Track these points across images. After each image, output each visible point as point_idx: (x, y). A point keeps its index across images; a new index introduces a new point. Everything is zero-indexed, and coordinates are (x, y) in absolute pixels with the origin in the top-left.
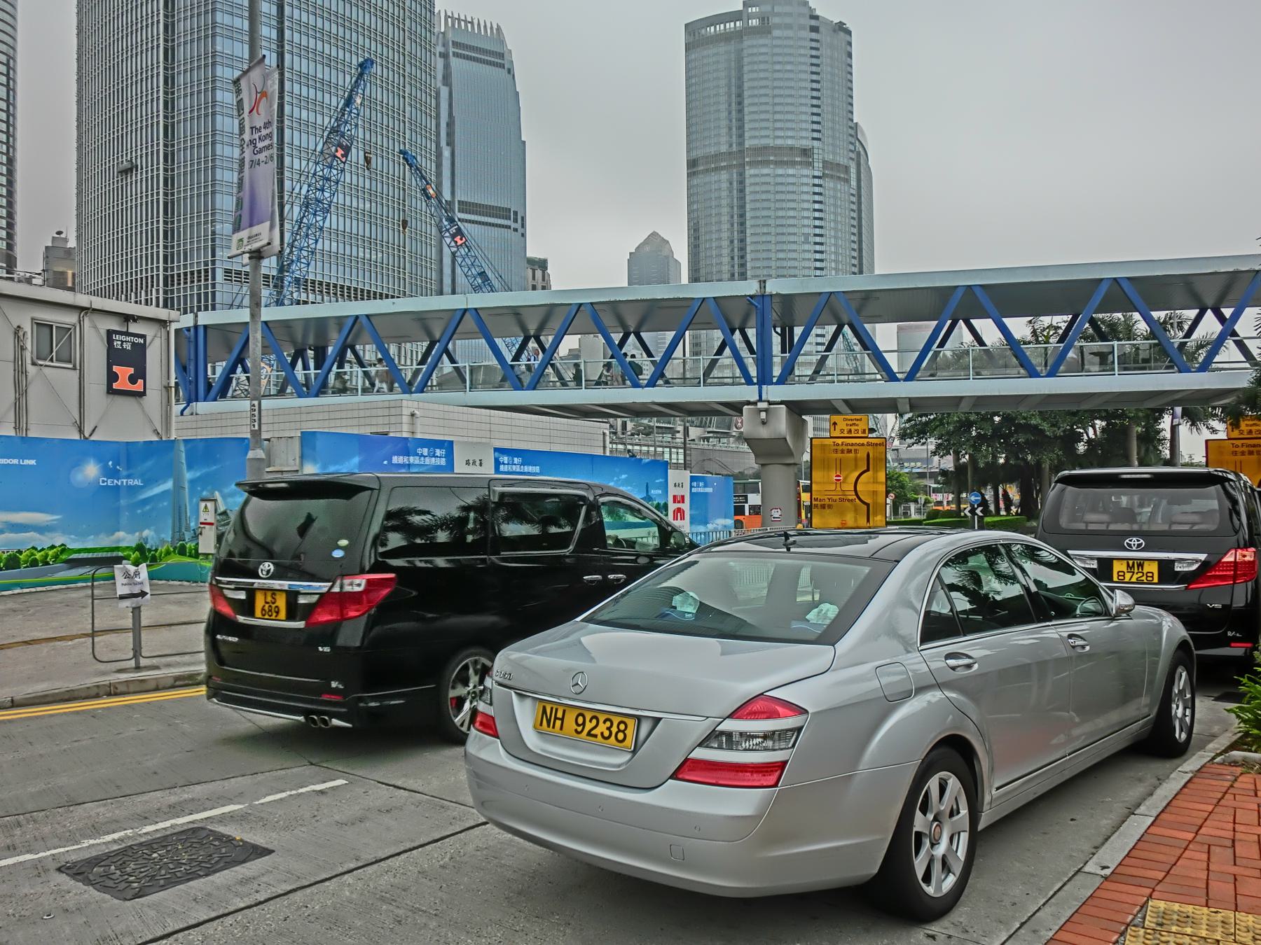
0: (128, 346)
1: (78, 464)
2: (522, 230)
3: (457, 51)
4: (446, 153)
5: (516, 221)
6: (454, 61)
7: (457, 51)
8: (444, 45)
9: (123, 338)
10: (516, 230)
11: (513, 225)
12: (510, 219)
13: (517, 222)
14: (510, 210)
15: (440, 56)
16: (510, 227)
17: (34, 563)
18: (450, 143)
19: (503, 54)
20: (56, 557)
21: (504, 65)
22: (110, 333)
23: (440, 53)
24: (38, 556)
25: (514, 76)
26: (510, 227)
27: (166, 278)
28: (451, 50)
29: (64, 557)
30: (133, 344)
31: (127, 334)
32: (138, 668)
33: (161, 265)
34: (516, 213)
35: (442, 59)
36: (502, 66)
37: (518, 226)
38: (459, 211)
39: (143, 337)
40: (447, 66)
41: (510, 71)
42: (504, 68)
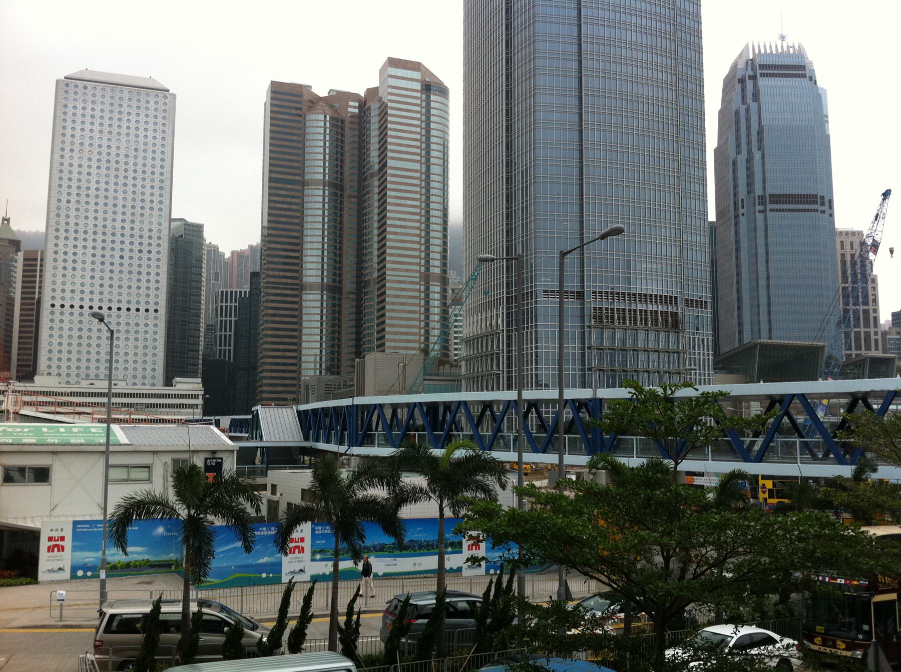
0: (213, 464)
1: (155, 527)
2: (828, 211)
3: (763, 71)
4: (757, 156)
5: (823, 204)
6: (762, 82)
7: (763, 71)
8: (752, 70)
9: (211, 461)
10: (823, 212)
11: (821, 208)
12: (817, 204)
13: (824, 205)
14: (816, 195)
15: (749, 79)
16: (817, 210)
17: (136, 566)
18: (761, 148)
19: (804, 66)
20: (145, 564)
21: (805, 74)
22: (206, 459)
23: (749, 76)
24: (137, 563)
25: (815, 81)
26: (817, 210)
27: (508, 298)
28: (759, 72)
29: (148, 564)
30: (216, 462)
31: (214, 458)
32: (61, 621)
33: (505, 290)
34: (822, 198)
35: (740, 85)
36: (804, 76)
37: (826, 208)
38: (770, 203)
39: (222, 459)
40: (756, 86)
41: (811, 79)
42: (806, 77)
